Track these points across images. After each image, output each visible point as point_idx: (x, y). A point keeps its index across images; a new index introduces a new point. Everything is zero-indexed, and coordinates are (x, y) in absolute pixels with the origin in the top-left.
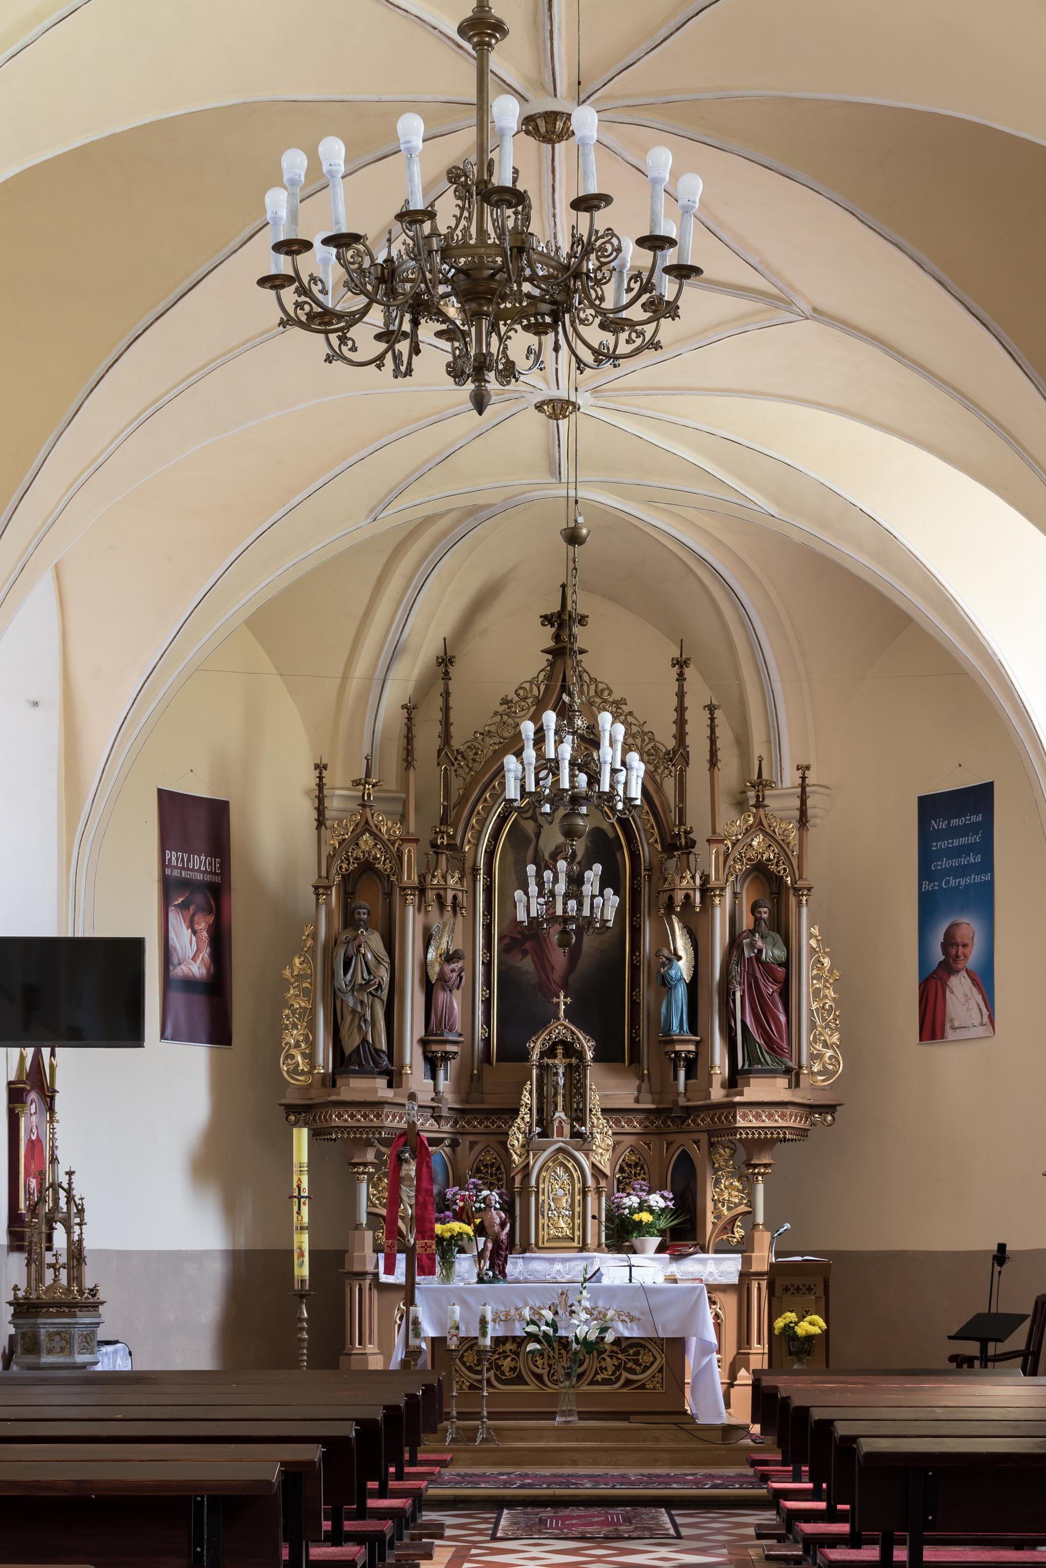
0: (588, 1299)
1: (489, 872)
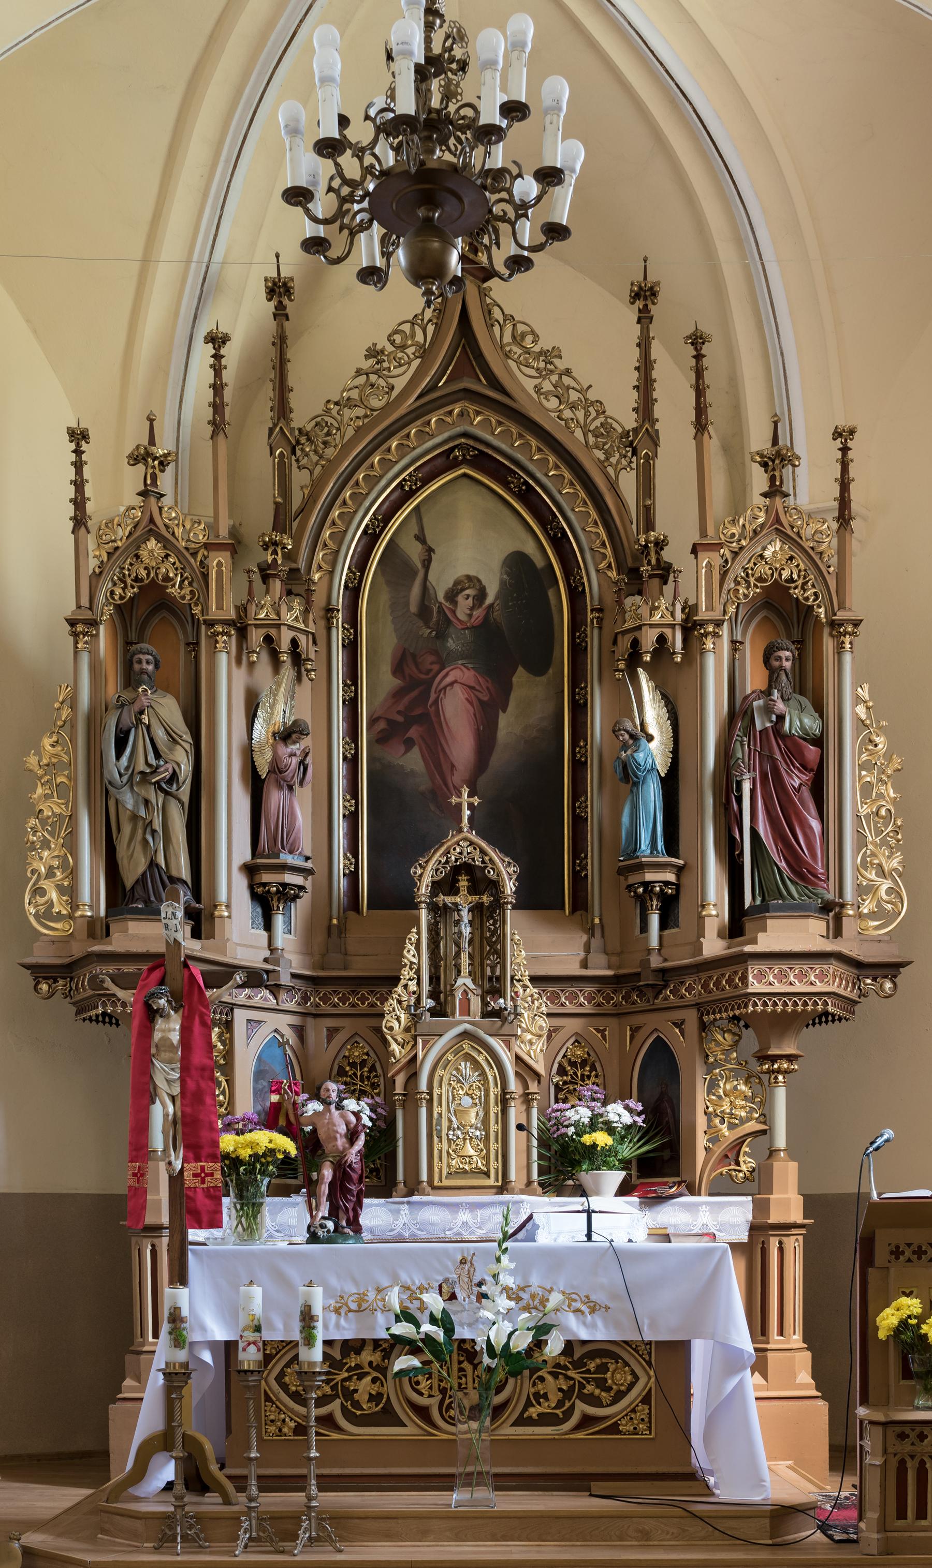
0: (512, 1273)
1: (353, 620)
